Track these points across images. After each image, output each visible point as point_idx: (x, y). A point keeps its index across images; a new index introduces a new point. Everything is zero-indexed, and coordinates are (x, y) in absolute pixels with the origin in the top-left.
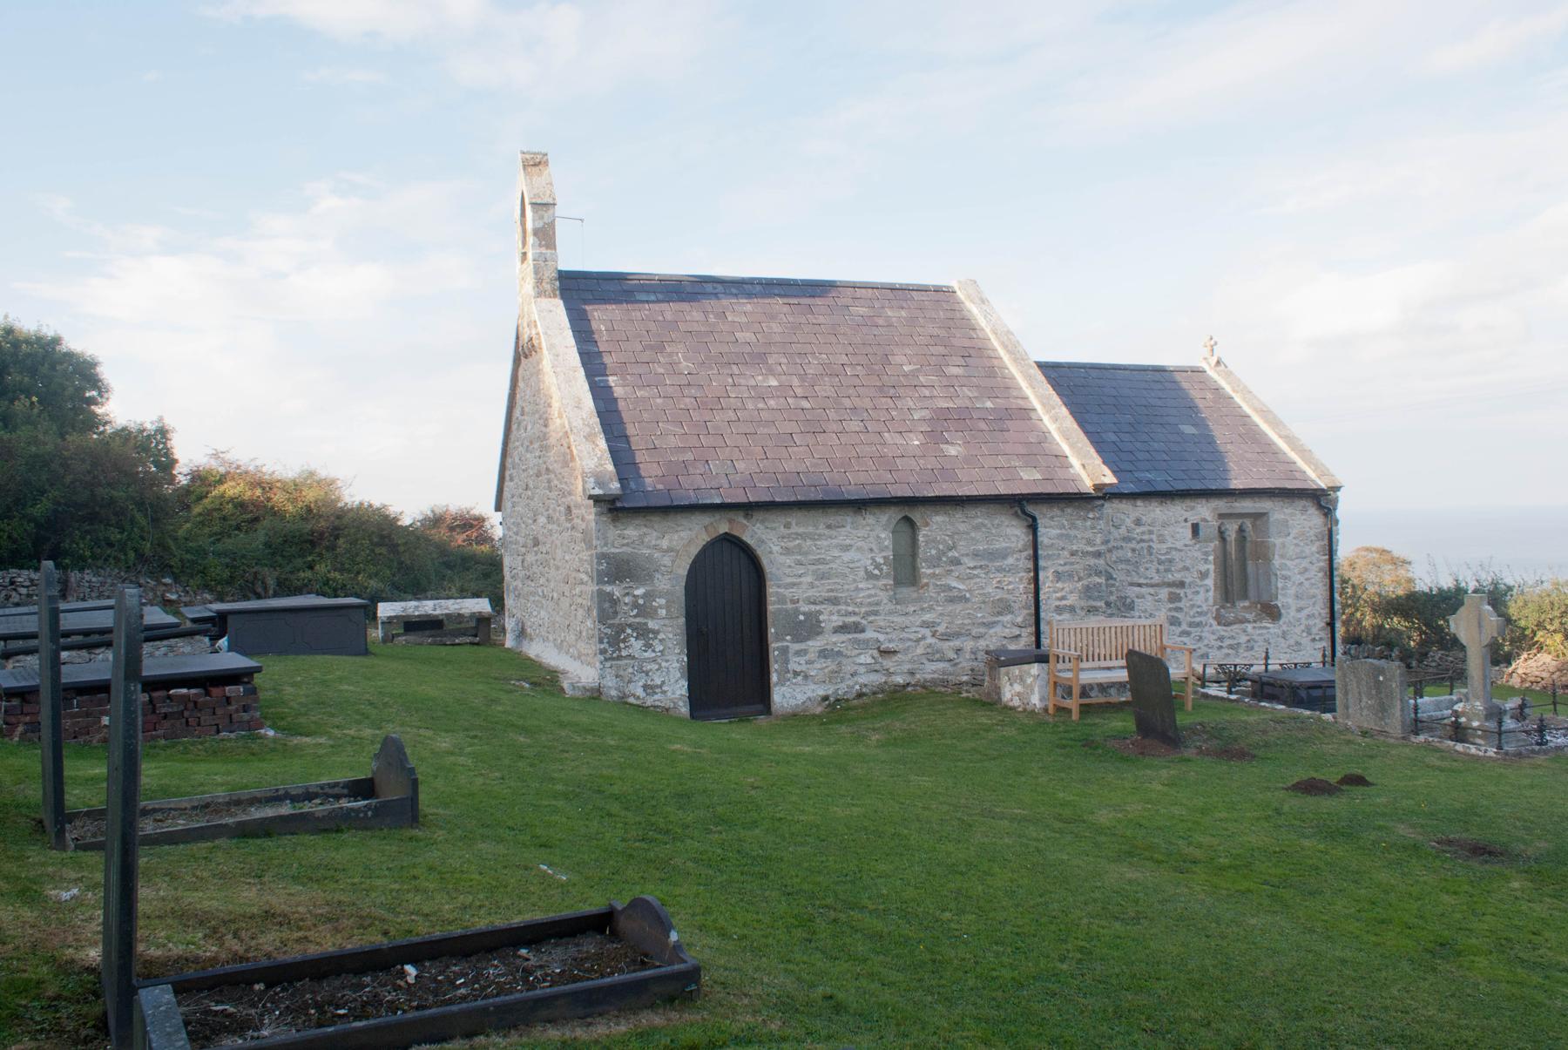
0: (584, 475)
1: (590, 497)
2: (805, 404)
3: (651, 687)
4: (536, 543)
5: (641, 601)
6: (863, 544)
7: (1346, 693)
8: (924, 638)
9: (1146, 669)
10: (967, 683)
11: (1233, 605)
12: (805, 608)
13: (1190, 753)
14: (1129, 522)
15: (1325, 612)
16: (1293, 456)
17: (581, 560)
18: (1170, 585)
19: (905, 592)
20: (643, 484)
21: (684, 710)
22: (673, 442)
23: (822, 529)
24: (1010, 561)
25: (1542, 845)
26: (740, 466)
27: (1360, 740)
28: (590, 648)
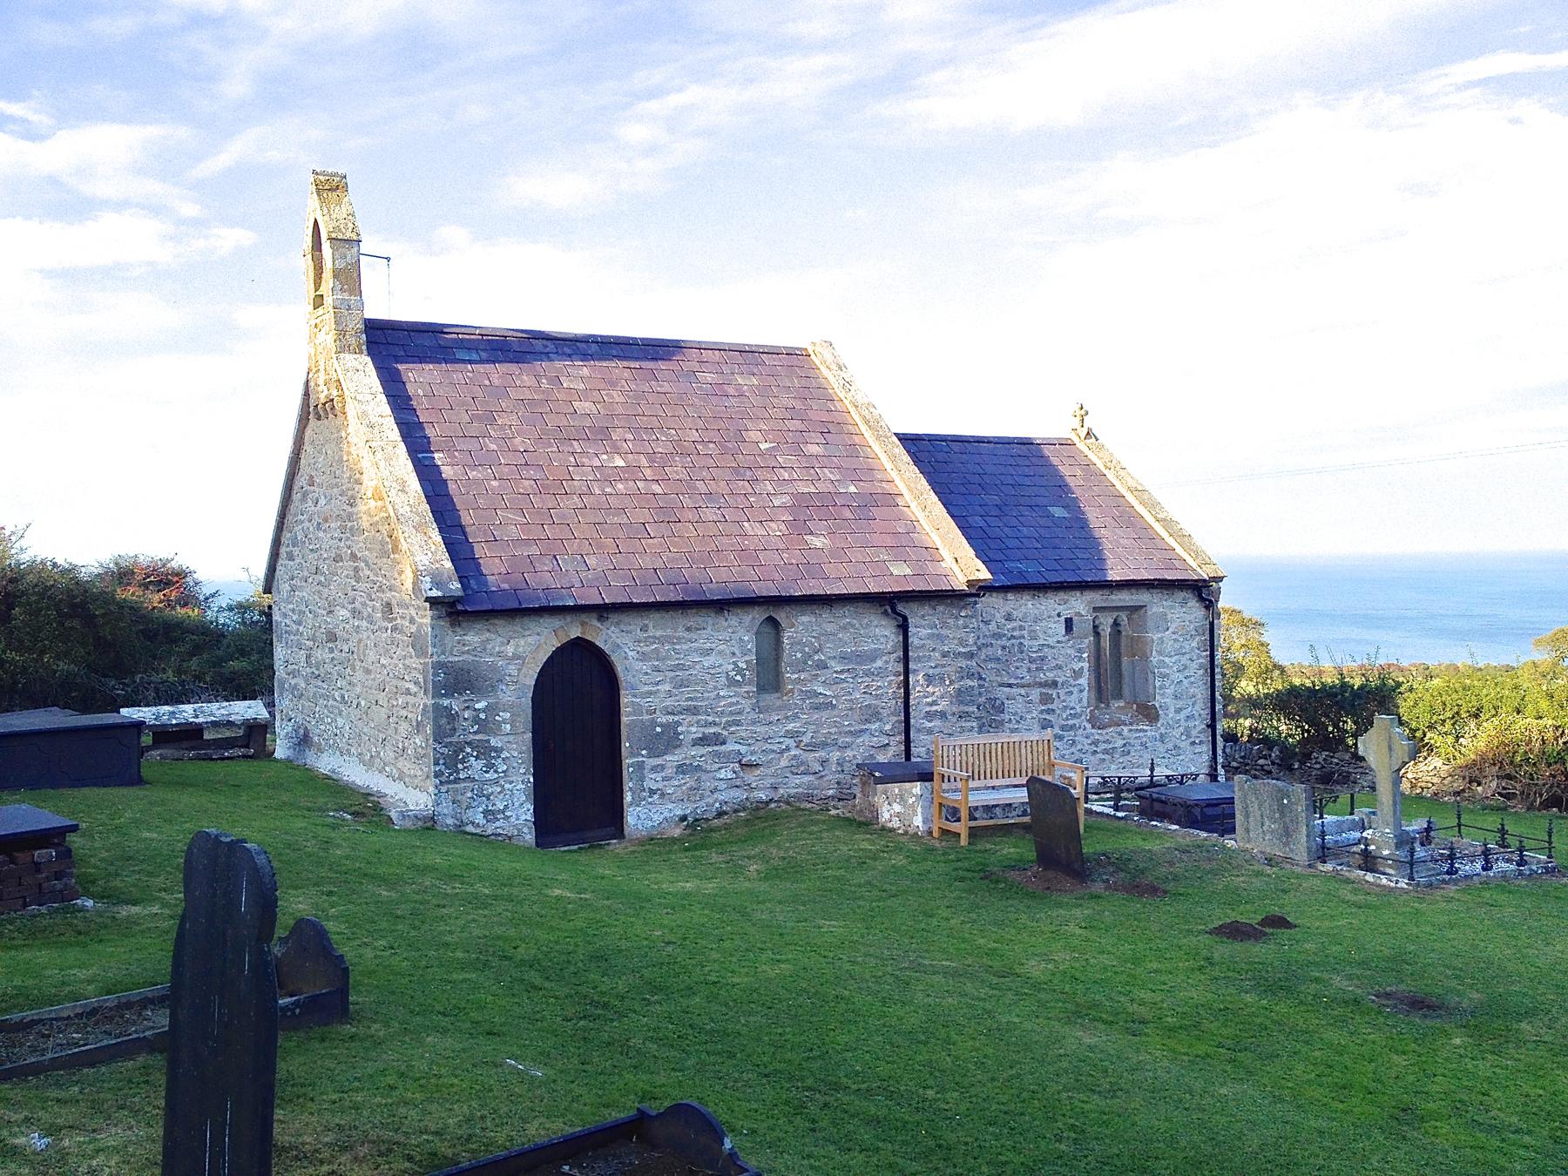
0: (417, 575)
1: (427, 599)
2: (657, 489)
3: (493, 813)
4: (332, 637)
5: (483, 716)
6: (727, 646)
7: (1247, 816)
8: (788, 749)
9: (1048, 798)
10: (833, 797)
11: (1108, 706)
12: (663, 719)
13: (1098, 887)
14: (999, 617)
15: (1206, 713)
16: (1171, 542)
17: (406, 667)
18: (1041, 685)
19: (770, 699)
20: (486, 583)
21: (529, 837)
22: (514, 532)
23: (681, 633)
24: (879, 663)
25: (1476, 996)
26: (592, 561)
27: (1268, 870)
28: (421, 770)
